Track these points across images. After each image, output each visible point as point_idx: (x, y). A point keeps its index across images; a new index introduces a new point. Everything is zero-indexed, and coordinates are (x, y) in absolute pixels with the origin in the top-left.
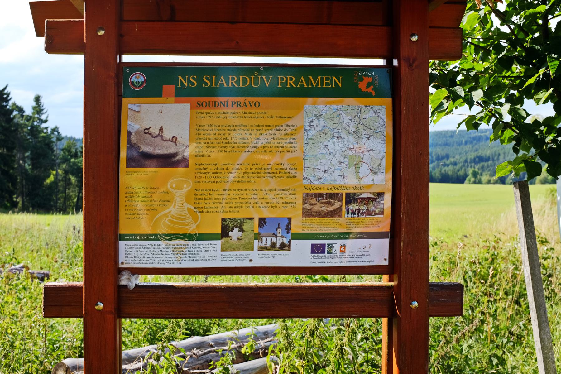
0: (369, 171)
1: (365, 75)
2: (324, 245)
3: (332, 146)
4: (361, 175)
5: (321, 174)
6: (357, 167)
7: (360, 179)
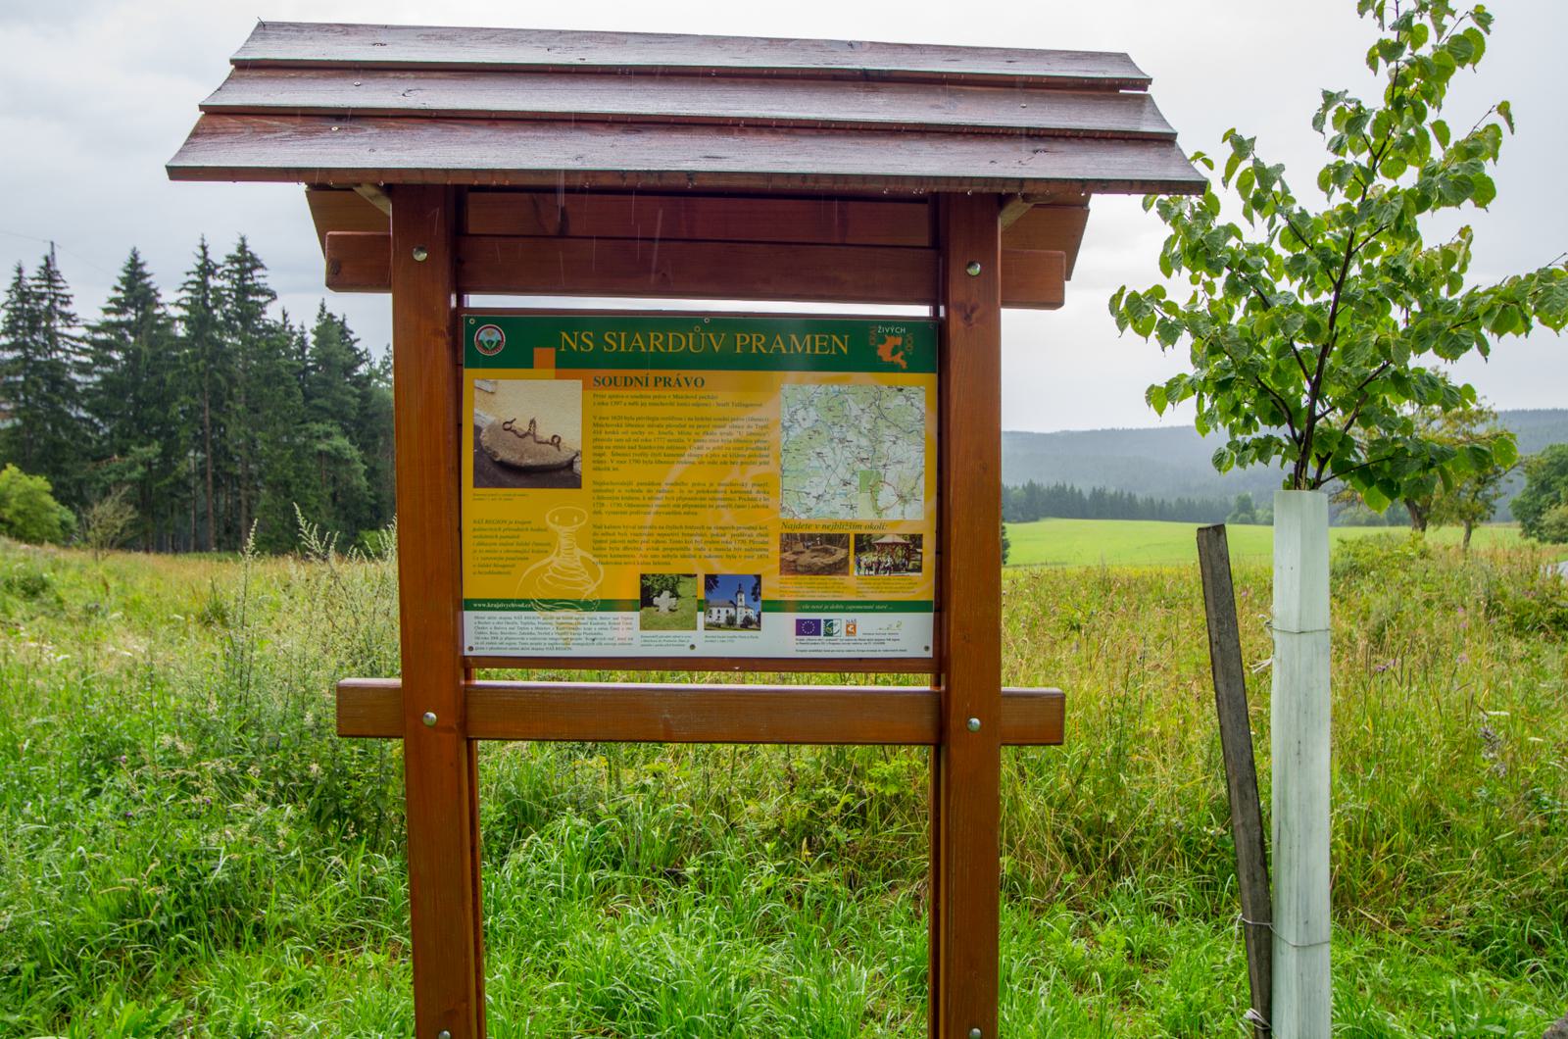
0: (895, 498)
1: (890, 334)
2: (817, 622)
3: (831, 454)
4: (881, 504)
5: (811, 502)
6: (873, 491)
7: (879, 512)
